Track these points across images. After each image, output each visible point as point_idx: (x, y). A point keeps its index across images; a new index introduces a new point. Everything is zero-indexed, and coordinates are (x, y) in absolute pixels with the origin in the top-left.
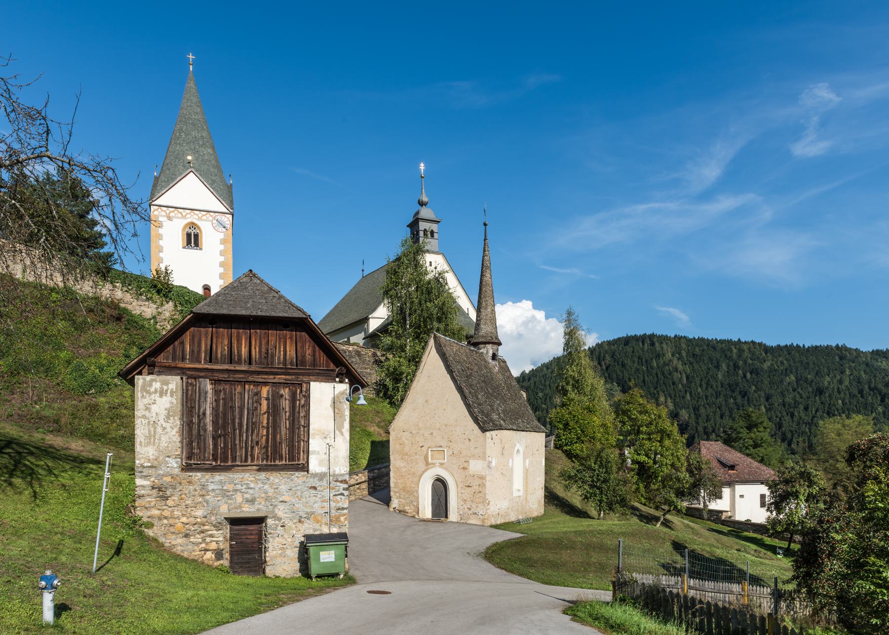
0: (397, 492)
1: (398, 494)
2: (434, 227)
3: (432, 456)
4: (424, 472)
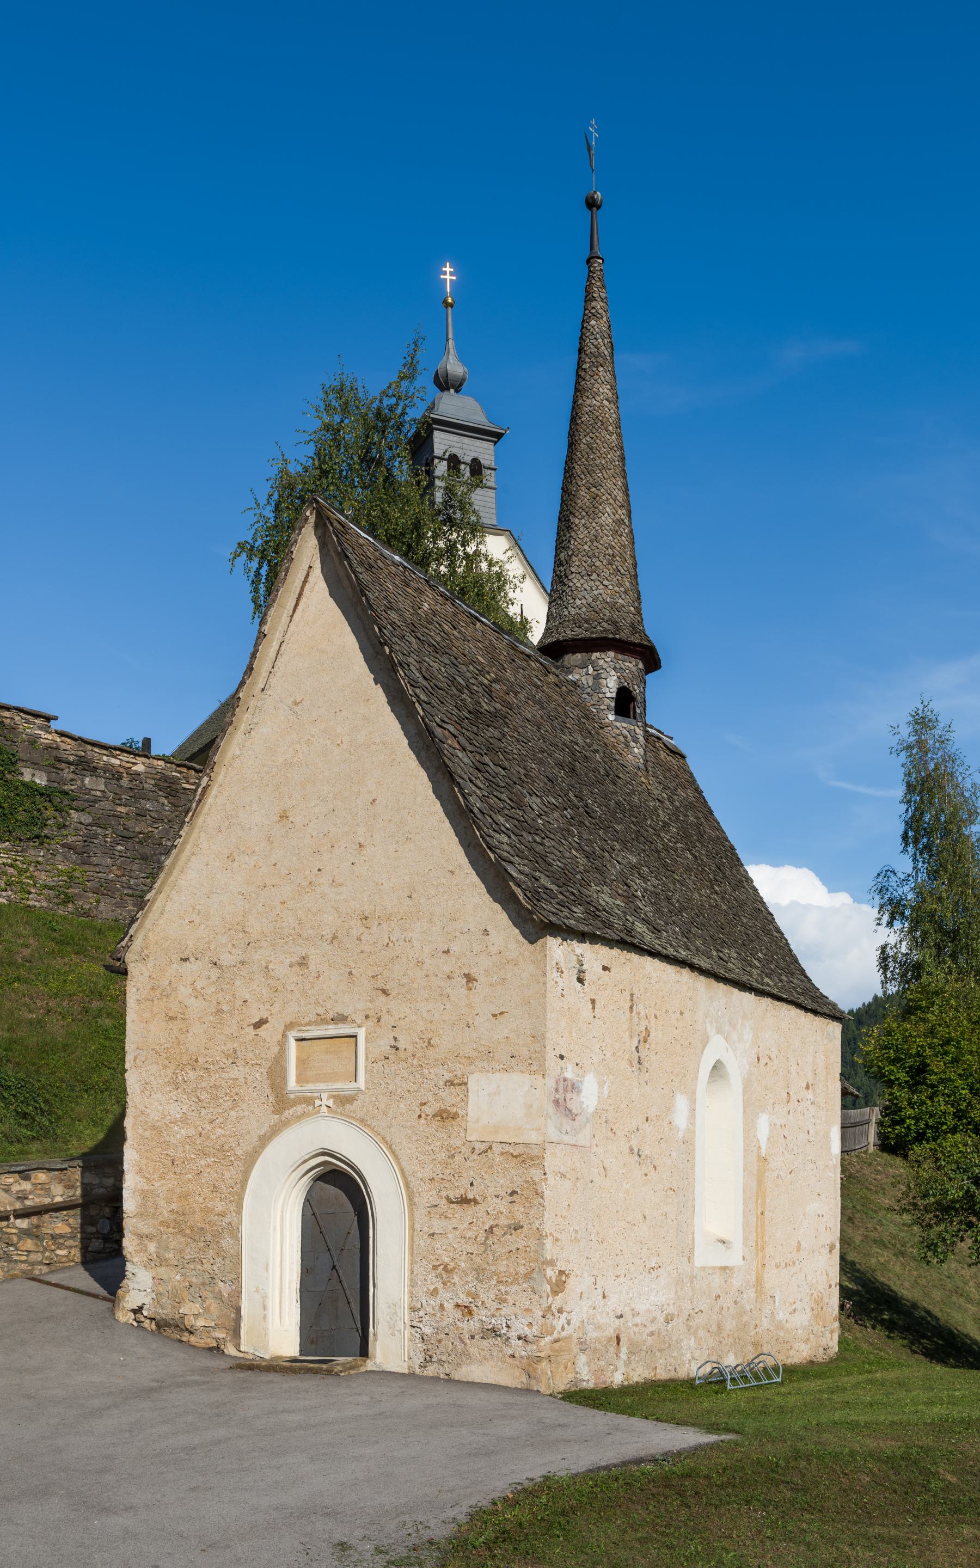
0: (149, 1237)
1: (152, 1247)
2: (483, 451)
3: (302, 1063)
4: (264, 1140)
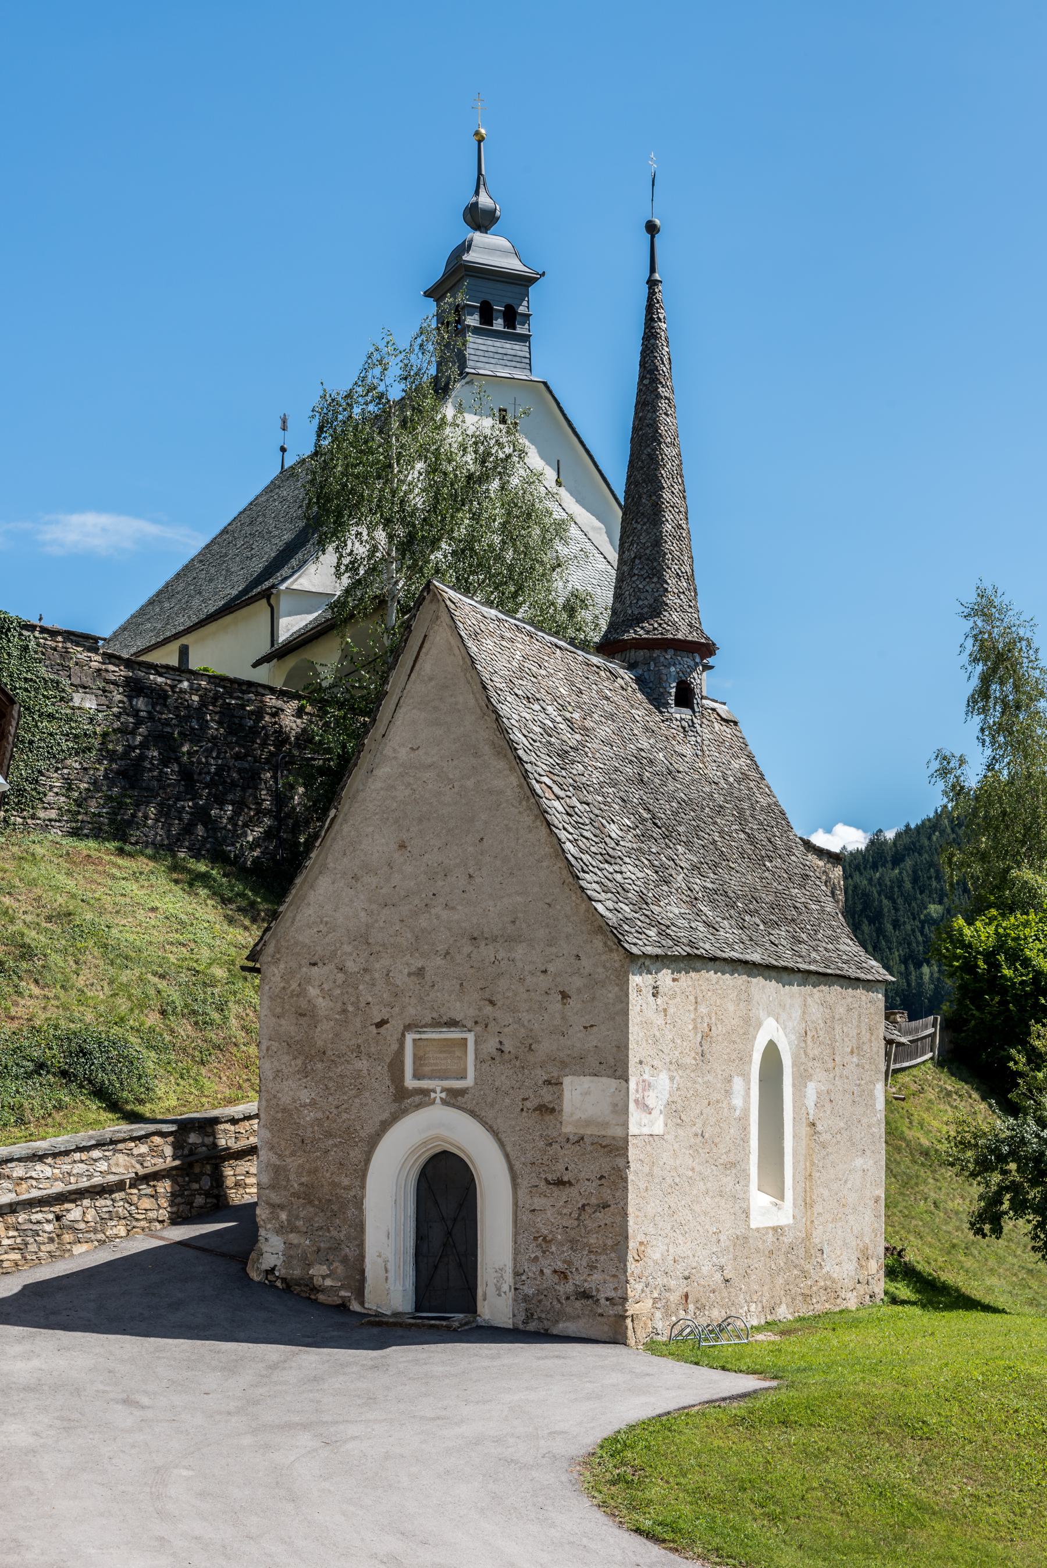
0: (281, 1207)
4: (385, 1126)
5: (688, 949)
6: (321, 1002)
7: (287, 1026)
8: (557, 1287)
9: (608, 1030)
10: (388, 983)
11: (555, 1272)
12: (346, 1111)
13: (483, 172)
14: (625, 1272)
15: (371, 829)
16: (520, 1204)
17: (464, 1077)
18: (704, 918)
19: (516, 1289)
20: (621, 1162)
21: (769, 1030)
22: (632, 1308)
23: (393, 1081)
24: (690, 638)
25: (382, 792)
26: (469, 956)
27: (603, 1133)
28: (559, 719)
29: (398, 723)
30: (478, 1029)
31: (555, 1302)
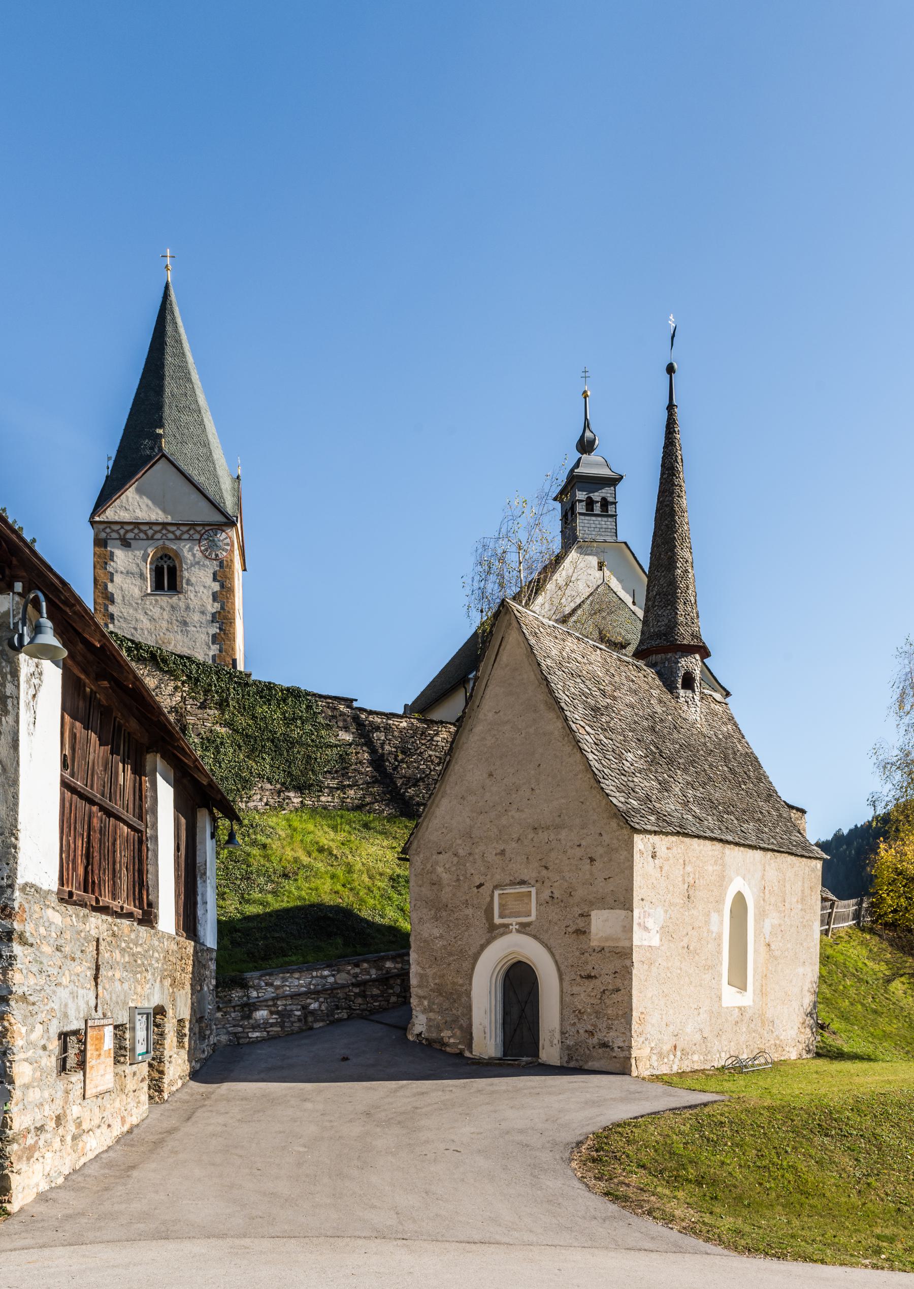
0: (425, 998)
4: (483, 947)
5: (678, 829)
6: (445, 876)
7: (426, 891)
8: (587, 1041)
9: (620, 880)
10: (483, 861)
11: (586, 1031)
12: (461, 939)
13: (588, 417)
14: (630, 1030)
15: (472, 766)
16: (565, 990)
17: (529, 915)
18: (693, 813)
19: (562, 1042)
20: (628, 962)
21: (737, 885)
22: (634, 1053)
23: (487, 920)
24: (692, 643)
25: (478, 743)
26: (532, 840)
27: (617, 945)
28: (595, 689)
29: (487, 697)
30: (538, 885)
31: (586, 1050)
